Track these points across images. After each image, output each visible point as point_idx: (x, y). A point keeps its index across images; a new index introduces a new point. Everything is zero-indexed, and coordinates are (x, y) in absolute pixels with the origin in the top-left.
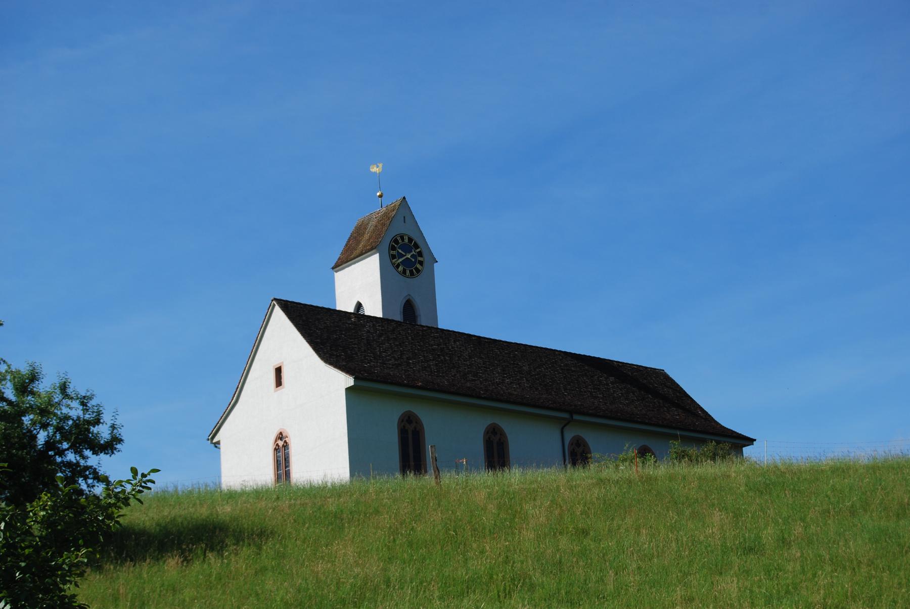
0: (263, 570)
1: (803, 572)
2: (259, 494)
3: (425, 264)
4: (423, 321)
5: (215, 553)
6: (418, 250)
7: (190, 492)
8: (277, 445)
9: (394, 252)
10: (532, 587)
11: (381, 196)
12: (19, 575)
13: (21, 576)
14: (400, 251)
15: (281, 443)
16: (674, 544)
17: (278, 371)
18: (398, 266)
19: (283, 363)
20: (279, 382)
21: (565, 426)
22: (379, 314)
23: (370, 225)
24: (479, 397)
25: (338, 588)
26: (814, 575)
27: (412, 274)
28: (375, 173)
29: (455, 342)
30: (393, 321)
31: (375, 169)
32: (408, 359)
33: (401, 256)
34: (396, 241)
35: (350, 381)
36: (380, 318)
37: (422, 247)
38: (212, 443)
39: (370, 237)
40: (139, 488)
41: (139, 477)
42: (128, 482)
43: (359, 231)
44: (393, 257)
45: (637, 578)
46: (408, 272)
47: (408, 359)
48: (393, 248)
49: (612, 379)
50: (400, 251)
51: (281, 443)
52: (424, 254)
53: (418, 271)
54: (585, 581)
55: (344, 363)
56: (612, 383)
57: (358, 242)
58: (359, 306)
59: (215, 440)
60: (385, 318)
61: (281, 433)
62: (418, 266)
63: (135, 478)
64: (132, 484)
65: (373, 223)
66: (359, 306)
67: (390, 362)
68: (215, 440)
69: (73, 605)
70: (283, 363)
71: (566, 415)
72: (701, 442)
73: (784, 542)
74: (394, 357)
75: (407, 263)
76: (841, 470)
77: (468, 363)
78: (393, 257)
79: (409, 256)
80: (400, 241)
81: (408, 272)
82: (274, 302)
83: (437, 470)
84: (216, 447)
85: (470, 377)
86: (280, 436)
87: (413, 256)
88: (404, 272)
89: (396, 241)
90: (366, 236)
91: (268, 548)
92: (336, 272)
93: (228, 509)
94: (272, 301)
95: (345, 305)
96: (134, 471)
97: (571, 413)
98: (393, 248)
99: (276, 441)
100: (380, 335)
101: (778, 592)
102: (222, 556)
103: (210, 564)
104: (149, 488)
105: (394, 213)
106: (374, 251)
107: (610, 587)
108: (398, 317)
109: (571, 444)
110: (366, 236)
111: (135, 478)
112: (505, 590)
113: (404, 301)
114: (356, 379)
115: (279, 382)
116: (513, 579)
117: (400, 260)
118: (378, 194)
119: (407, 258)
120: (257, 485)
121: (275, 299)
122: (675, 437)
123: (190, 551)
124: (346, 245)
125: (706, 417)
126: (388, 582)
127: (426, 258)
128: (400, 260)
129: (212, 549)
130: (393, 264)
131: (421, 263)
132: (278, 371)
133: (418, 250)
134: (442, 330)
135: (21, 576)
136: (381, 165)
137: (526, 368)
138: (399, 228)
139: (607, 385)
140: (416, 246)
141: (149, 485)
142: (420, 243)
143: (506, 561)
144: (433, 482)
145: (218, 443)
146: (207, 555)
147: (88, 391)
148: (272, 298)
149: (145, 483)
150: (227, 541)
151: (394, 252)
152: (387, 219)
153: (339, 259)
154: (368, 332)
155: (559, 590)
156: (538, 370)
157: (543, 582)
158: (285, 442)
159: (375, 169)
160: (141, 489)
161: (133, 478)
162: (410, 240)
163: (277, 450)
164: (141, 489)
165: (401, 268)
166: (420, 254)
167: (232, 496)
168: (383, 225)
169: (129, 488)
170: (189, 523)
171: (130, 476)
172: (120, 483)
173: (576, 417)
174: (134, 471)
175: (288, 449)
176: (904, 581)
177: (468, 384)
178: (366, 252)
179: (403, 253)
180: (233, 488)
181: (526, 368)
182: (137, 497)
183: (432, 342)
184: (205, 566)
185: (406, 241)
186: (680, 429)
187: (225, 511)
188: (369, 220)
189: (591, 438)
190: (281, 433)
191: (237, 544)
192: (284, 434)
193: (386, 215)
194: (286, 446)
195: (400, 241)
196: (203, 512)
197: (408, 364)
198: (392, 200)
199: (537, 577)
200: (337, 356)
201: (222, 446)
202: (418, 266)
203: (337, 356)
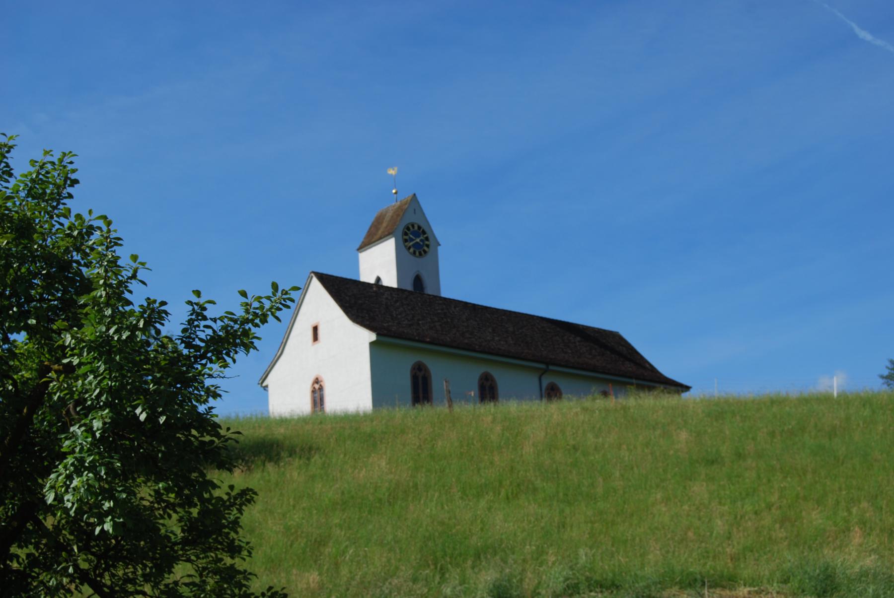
0: (313, 478)
1: (759, 477)
2: (303, 421)
3: (431, 247)
4: (429, 291)
5: (272, 464)
6: (425, 236)
7: (251, 418)
8: (314, 388)
9: (406, 237)
10: (535, 490)
11: (396, 193)
12: (153, 386)
13: (156, 387)
14: (411, 236)
15: (317, 386)
16: (650, 457)
17: (315, 329)
18: (409, 248)
19: (319, 322)
20: (316, 338)
21: (542, 374)
22: (394, 285)
23: (387, 215)
24: (475, 351)
25: (376, 490)
26: (769, 481)
27: (420, 254)
28: (392, 175)
29: (455, 308)
30: (406, 291)
31: (392, 172)
32: (419, 320)
33: (412, 240)
34: (408, 229)
35: (373, 337)
36: (395, 288)
37: (429, 234)
38: (262, 386)
39: (386, 227)
40: (278, 305)
41: (279, 294)
42: (269, 298)
43: (378, 221)
44: (406, 241)
45: (621, 483)
46: (417, 253)
47: (419, 320)
48: (406, 234)
49: (578, 339)
50: (411, 236)
51: (317, 386)
52: (431, 239)
53: (425, 252)
54: (579, 486)
55: (368, 323)
56: (579, 342)
57: (378, 229)
58: (378, 279)
59: (264, 384)
60: (400, 287)
61: (317, 379)
62: (426, 248)
63: (274, 295)
64: (271, 301)
65: (390, 214)
66: (378, 279)
67: (405, 323)
68: (264, 384)
69: (103, 589)
70: (319, 322)
71: (542, 366)
72: (650, 389)
73: (739, 456)
74: (407, 319)
75: (417, 245)
76: (775, 402)
77: (466, 324)
78: (406, 241)
79: (418, 240)
80: (411, 228)
81: (417, 253)
82: (312, 275)
83: (450, 401)
84: (265, 390)
85: (467, 335)
86: (317, 381)
87: (421, 240)
88: (414, 253)
89: (408, 229)
90: (384, 225)
91: (316, 458)
92: (361, 252)
93: (282, 431)
94: (311, 273)
95: (367, 276)
96: (275, 287)
97: (547, 364)
98: (406, 234)
99: (313, 384)
100: (396, 302)
101: (741, 494)
102: (279, 466)
103: (268, 472)
104: (288, 307)
105: (406, 206)
106: (391, 236)
107: (600, 490)
108: (409, 287)
109: (547, 389)
110: (384, 225)
111: (274, 295)
112: (512, 493)
113: (415, 276)
114: (378, 335)
115: (316, 338)
116: (519, 485)
117: (411, 243)
118: (394, 191)
119: (417, 243)
120: (303, 412)
121: (313, 272)
122: (632, 384)
123: (252, 462)
124: (369, 232)
125: (653, 370)
126: (416, 486)
127: (431, 242)
128: (411, 243)
129: (270, 460)
130: (406, 246)
131: (428, 246)
132: (315, 329)
133: (425, 236)
134: (445, 299)
135: (156, 387)
136: (396, 169)
137: (511, 329)
138: (410, 219)
139: (575, 343)
140: (424, 232)
141: (289, 303)
142: (426, 230)
143: (512, 469)
144: (447, 410)
145: (267, 386)
146: (266, 465)
147: (168, 332)
148: (311, 271)
149: (284, 299)
150: (282, 454)
151: (406, 237)
152: (401, 211)
153: (363, 242)
154: (387, 299)
155: (558, 492)
156: (520, 331)
157: (544, 487)
158: (321, 385)
159: (392, 172)
160: (281, 306)
161: (273, 295)
162: (419, 228)
163: (314, 391)
164: (281, 306)
165: (412, 250)
166: (427, 239)
167: (283, 421)
168: (398, 215)
169: (267, 304)
170: (250, 441)
171: (269, 292)
172: (259, 299)
173: (551, 367)
174: (275, 287)
175: (323, 391)
176: (843, 486)
177: (466, 341)
178: (384, 237)
179: (414, 238)
180: (283, 416)
181: (511, 329)
182: (276, 315)
183: (437, 308)
184: (265, 474)
185: (416, 228)
186: (637, 378)
187: (279, 432)
188: (387, 212)
189: (561, 383)
190: (317, 379)
191: (290, 456)
192: (320, 379)
193: (400, 207)
194: (321, 389)
195: (411, 228)
196: (261, 433)
197: (419, 324)
198: (406, 196)
199: (538, 483)
200: (362, 317)
201: (270, 389)
202: (426, 248)
203: (362, 317)
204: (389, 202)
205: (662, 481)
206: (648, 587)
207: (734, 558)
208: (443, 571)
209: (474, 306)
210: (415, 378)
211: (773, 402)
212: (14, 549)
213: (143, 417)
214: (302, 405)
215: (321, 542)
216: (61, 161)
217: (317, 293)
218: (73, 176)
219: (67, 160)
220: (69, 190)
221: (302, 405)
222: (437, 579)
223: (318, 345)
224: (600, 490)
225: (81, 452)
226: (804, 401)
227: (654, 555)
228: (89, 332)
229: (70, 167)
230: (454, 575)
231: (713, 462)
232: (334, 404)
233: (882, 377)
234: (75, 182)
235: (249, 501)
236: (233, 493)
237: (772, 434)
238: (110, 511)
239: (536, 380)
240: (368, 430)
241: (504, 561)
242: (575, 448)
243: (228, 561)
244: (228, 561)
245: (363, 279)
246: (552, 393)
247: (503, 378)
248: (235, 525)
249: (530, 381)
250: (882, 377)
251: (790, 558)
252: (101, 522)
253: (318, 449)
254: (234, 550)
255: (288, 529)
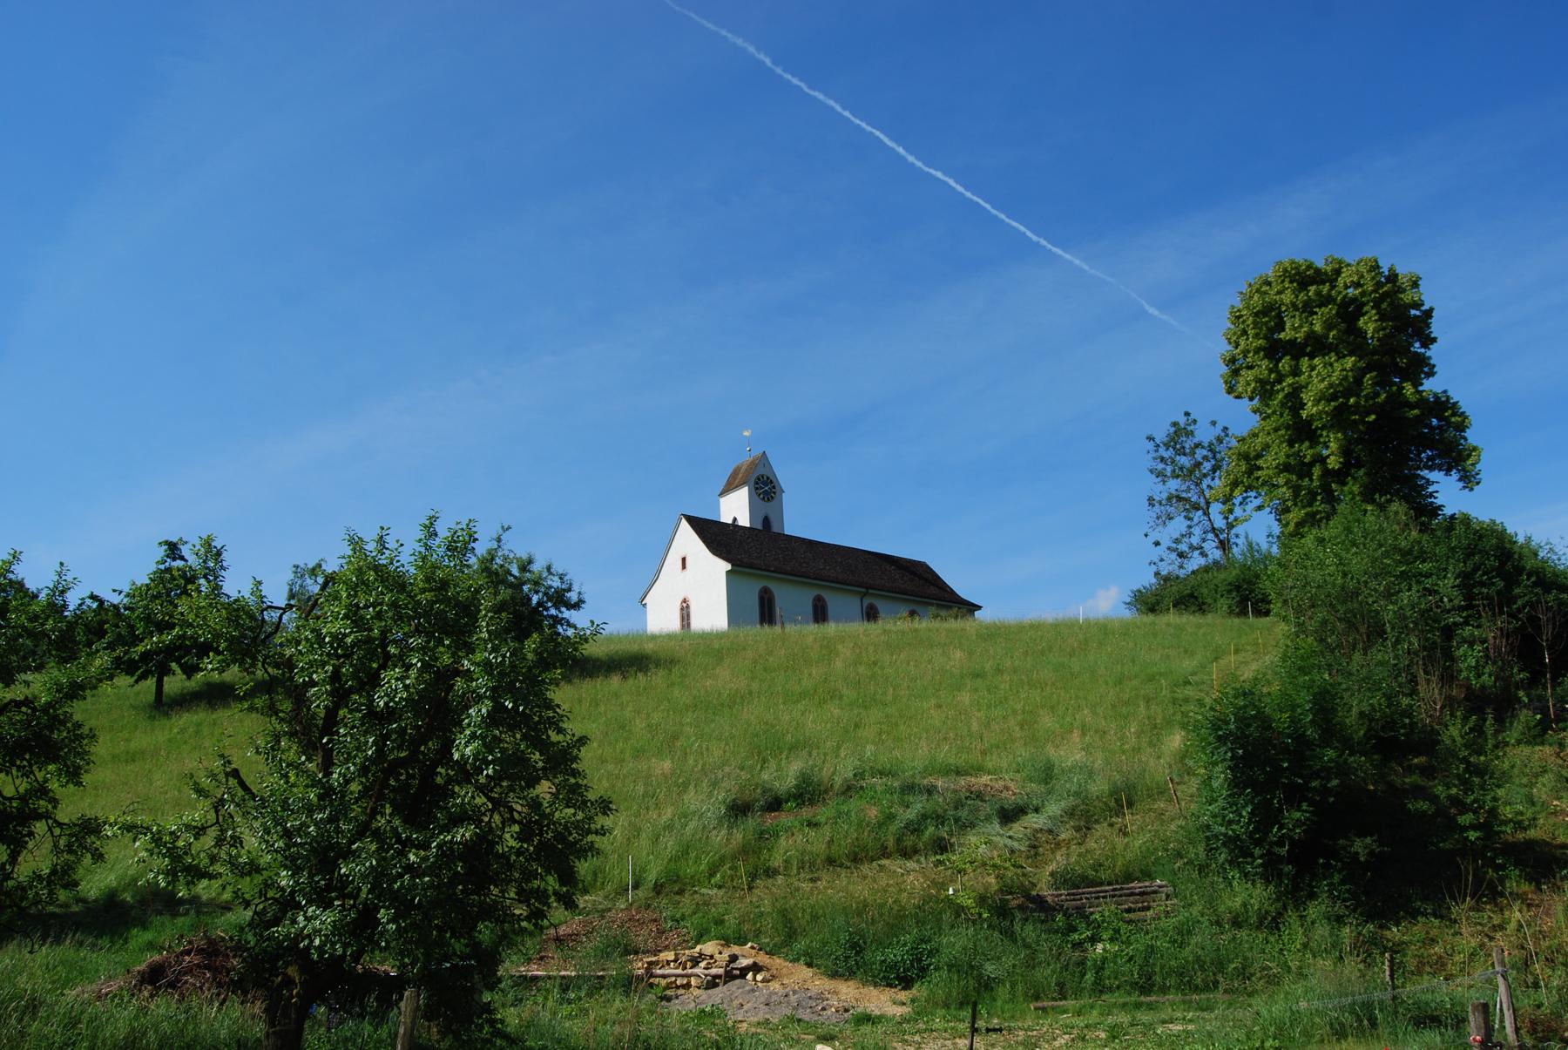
0: (673, 684)
2: (670, 637)
4: (775, 529)
15: (685, 605)
20: (684, 567)
22: (748, 525)
31: (746, 433)
33: (761, 488)
35: (729, 567)
43: (736, 472)
44: (757, 489)
58: (735, 519)
66: (735, 519)
71: (864, 590)
75: (766, 493)
78: (757, 489)
83: (783, 624)
85: (804, 565)
86: (685, 601)
90: (740, 476)
96: (592, 622)
97: (867, 588)
108: (759, 527)
110: (740, 476)
115: (684, 567)
121: (685, 516)
122: (932, 604)
126: (750, 693)
127: (777, 490)
129: (640, 671)
131: (774, 493)
138: (761, 471)
140: (771, 482)
152: (754, 465)
159: (746, 433)
162: (768, 478)
163: (682, 609)
166: (774, 487)
167: (653, 637)
171: (590, 625)
173: (870, 591)
174: (592, 622)
187: (649, 647)
188: (742, 465)
189: (879, 604)
191: (656, 667)
193: (752, 462)
194: (688, 607)
196: (635, 648)
198: (757, 452)
201: (648, 606)
204: (745, 458)
205: (937, 691)
206: (913, 776)
207: (984, 753)
208: (764, 761)
209: (811, 542)
210: (761, 599)
211: (1032, 626)
212: (439, 770)
213: (510, 706)
214: (672, 624)
215: (675, 737)
216: (468, 525)
217: (686, 533)
218: (476, 536)
219: (472, 524)
220: (473, 545)
221: (672, 624)
222: (759, 767)
223: (685, 572)
224: (890, 698)
225: (475, 726)
226: (1056, 626)
227: (923, 750)
228: (478, 657)
229: (474, 529)
230: (772, 764)
231: (978, 676)
232: (700, 623)
233: (1126, 603)
234: (476, 540)
235: (584, 744)
236: (575, 739)
237: (1026, 653)
238: (492, 762)
239: (858, 600)
240: (717, 647)
241: (810, 754)
242: (875, 663)
243: (573, 781)
244: (573, 781)
245: (723, 520)
246: (871, 615)
247: (834, 601)
248: (576, 759)
249: (852, 603)
250: (1126, 603)
251: (1023, 753)
252: (487, 769)
253: (679, 661)
254: (575, 773)
255: (649, 726)
